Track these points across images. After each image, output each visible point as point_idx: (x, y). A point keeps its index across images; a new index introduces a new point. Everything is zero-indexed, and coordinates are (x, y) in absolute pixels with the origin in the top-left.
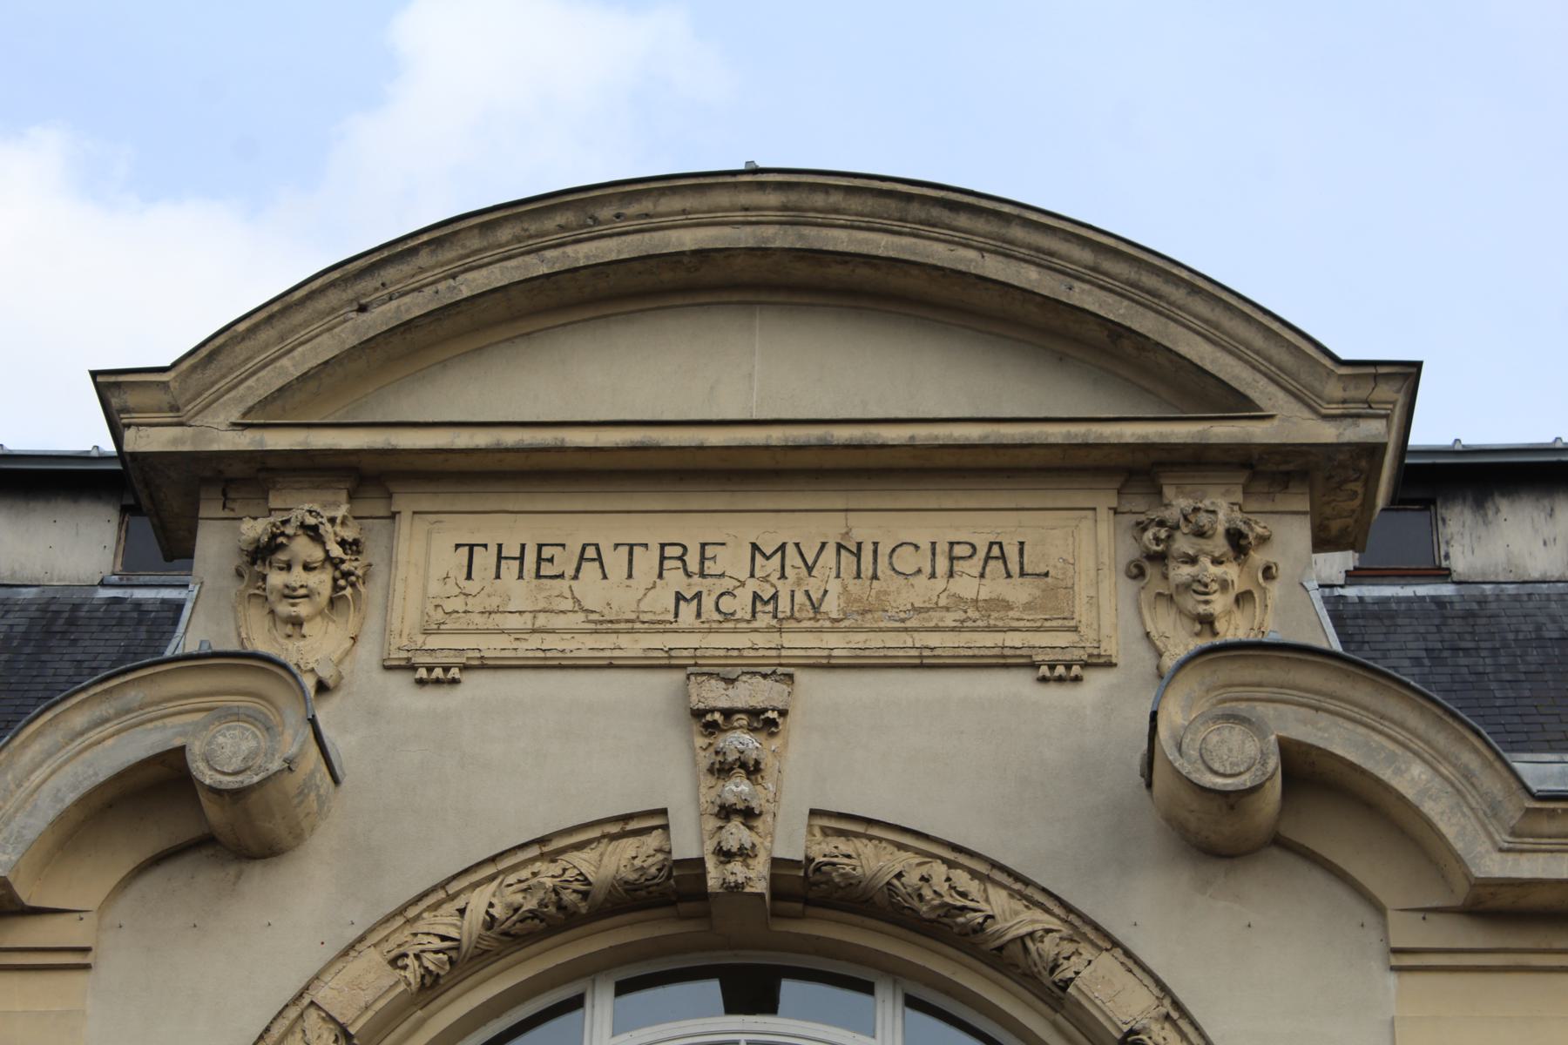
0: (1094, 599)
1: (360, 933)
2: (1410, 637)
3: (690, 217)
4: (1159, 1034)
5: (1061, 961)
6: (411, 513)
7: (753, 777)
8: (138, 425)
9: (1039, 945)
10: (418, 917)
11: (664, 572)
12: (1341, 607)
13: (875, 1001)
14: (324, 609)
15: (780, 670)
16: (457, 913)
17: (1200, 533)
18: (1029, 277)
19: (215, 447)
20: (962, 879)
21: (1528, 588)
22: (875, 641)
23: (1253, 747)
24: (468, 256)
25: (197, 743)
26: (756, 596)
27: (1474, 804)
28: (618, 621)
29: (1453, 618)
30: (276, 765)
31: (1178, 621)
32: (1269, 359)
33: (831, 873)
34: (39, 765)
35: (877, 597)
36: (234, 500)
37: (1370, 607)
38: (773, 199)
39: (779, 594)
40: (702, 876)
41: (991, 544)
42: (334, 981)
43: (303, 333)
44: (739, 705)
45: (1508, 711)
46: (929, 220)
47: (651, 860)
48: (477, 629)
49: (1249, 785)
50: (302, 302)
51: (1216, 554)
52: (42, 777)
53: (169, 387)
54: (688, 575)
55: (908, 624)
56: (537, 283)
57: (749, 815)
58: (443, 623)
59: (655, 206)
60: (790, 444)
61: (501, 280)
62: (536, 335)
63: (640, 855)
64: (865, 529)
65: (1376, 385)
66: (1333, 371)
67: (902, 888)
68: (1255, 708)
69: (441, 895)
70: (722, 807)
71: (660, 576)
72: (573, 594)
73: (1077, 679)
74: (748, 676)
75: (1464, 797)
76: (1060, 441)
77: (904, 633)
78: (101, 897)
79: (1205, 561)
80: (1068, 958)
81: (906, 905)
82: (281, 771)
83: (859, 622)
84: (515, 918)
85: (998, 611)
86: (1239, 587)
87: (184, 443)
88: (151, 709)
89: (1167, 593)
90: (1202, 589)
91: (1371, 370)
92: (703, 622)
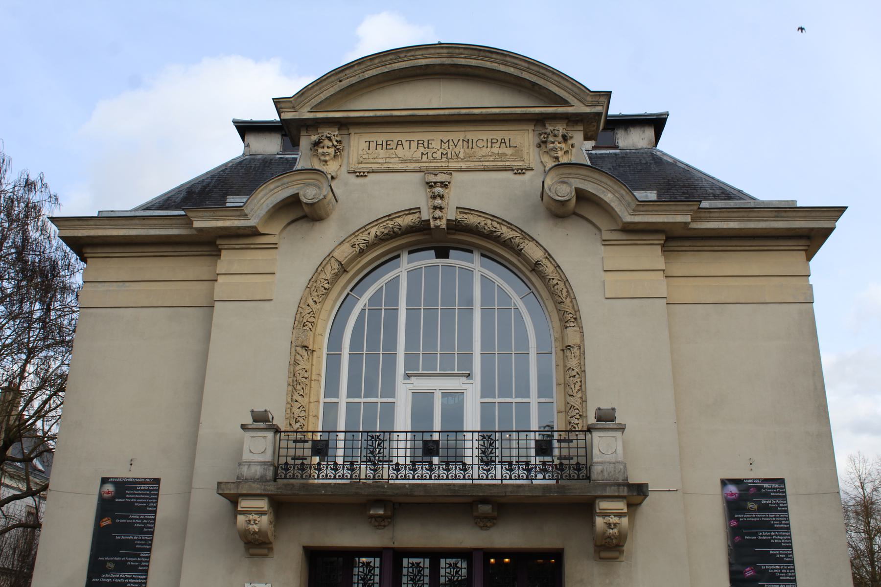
17: (555, 136)
18: (511, 70)
20: (495, 224)
22: (473, 164)
57: (441, 208)
79: (557, 143)
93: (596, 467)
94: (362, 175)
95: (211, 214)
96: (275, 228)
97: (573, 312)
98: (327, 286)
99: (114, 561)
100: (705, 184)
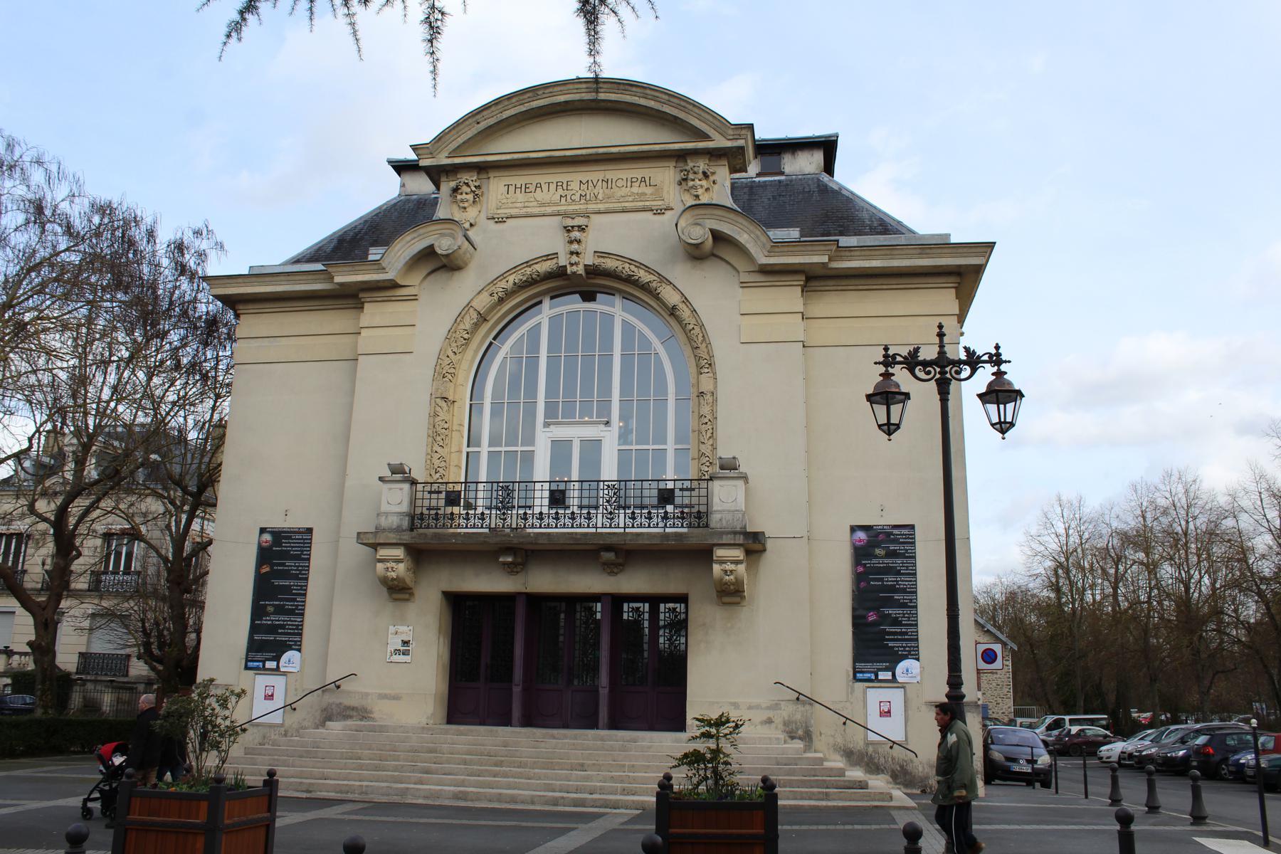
17: (695, 173)
18: (652, 104)
20: (633, 268)
22: (611, 205)
57: (577, 254)
78: (419, 282)
79: (697, 180)
93: (714, 516)
94: (501, 221)
95: (350, 269)
96: (415, 279)
97: (708, 358)
98: (466, 336)
99: (273, 605)
100: (865, 215)
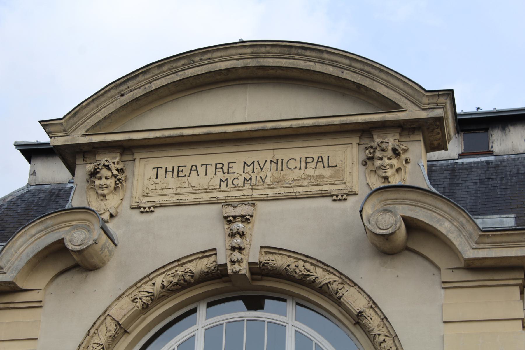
0: (351, 173)
1: (122, 292)
2: (476, 175)
3: (223, 58)
4: (368, 313)
5: (339, 290)
6: (139, 159)
7: (242, 237)
8: (54, 137)
9: (332, 286)
10: (141, 286)
11: (217, 173)
12: (455, 167)
13: (287, 305)
14: (112, 191)
15: (251, 202)
16: (153, 284)
17: (383, 150)
19: (77, 142)
20: (308, 266)
21: (519, 156)
22: (282, 191)
23: (392, 220)
24: (154, 76)
25: (68, 237)
26: (245, 179)
27: (464, 234)
28: (202, 189)
29: (491, 168)
30: (91, 242)
31: (378, 179)
32: (405, 92)
33: (267, 266)
34: (22, 246)
35: (283, 177)
36: (87, 158)
37: (465, 166)
38: (249, 50)
39: (252, 178)
40: (226, 269)
41: (319, 157)
42: (115, 308)
43: (104, 104)
44: (238, 214)
45: (501, 199)
46: (297, 54)
47: (212, 265)
48: (159, 195)
49: (390, 232)
50: (103, 95)
51: (389, 157)
52: (23, 249)
53: (63, 124)
54: (224, 173)
55: (292, 185)
56: (177, 83)
57: (240, 249)
58: (149, 193)
59: (212, 55)
60: (253, 130)
61: (165, 83)
62: (179, 99)
63: (208, 263)
64: (279, 155)
65: (439, 98)
66: (424, 94)
67: (289, 269)
68: (395, 206)
69: (147, 279)
70: (232, 247)
71: (215, 174)
72: (188, 182)
73: (345, 199)
74: (241, 205)
75: (461, 232)
76: (338, 123)
77: (291, 188)
79: (385, 159)
80: (341, 290)
81: (291, 275)
82: (93, 244)
83: (277, 185)
84: (171, 285)
85: (321, 179)
86: (396, 166)
87: (68, 142)
88: (55, 227)
89: (374, 170)
90: (384, 168)
91: (437, 93)
92: (228, 188)
94: (147, 210)
